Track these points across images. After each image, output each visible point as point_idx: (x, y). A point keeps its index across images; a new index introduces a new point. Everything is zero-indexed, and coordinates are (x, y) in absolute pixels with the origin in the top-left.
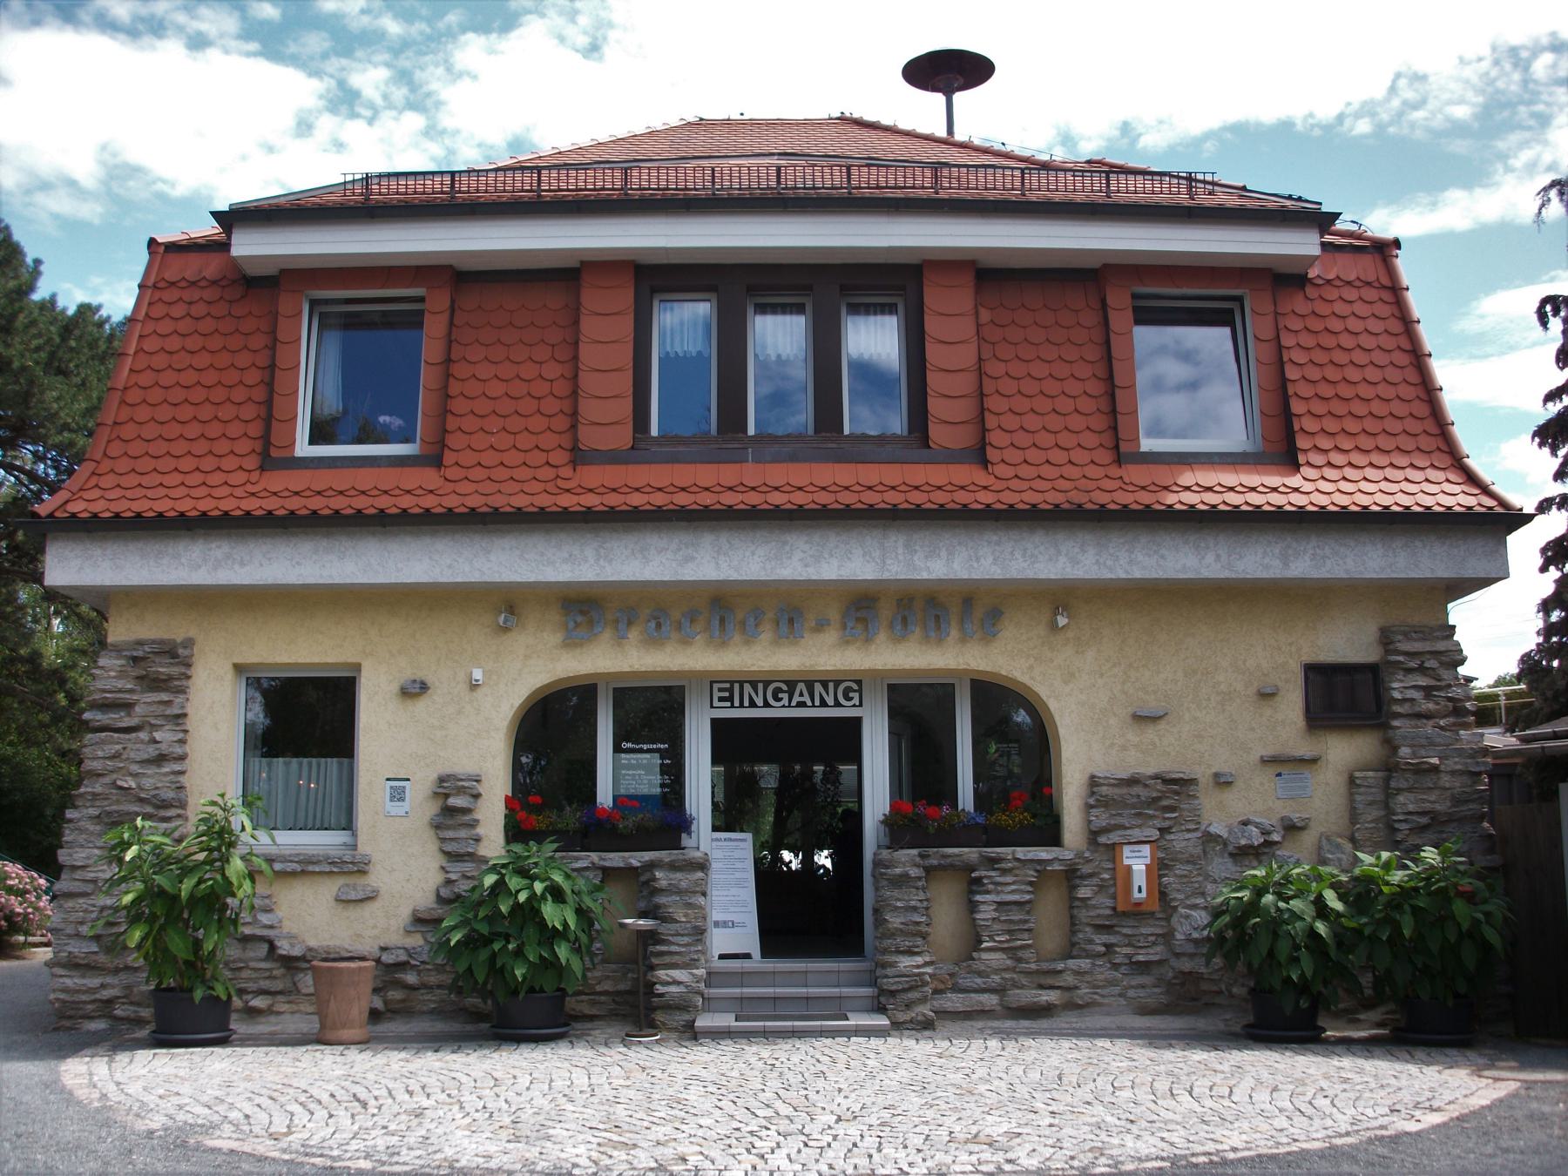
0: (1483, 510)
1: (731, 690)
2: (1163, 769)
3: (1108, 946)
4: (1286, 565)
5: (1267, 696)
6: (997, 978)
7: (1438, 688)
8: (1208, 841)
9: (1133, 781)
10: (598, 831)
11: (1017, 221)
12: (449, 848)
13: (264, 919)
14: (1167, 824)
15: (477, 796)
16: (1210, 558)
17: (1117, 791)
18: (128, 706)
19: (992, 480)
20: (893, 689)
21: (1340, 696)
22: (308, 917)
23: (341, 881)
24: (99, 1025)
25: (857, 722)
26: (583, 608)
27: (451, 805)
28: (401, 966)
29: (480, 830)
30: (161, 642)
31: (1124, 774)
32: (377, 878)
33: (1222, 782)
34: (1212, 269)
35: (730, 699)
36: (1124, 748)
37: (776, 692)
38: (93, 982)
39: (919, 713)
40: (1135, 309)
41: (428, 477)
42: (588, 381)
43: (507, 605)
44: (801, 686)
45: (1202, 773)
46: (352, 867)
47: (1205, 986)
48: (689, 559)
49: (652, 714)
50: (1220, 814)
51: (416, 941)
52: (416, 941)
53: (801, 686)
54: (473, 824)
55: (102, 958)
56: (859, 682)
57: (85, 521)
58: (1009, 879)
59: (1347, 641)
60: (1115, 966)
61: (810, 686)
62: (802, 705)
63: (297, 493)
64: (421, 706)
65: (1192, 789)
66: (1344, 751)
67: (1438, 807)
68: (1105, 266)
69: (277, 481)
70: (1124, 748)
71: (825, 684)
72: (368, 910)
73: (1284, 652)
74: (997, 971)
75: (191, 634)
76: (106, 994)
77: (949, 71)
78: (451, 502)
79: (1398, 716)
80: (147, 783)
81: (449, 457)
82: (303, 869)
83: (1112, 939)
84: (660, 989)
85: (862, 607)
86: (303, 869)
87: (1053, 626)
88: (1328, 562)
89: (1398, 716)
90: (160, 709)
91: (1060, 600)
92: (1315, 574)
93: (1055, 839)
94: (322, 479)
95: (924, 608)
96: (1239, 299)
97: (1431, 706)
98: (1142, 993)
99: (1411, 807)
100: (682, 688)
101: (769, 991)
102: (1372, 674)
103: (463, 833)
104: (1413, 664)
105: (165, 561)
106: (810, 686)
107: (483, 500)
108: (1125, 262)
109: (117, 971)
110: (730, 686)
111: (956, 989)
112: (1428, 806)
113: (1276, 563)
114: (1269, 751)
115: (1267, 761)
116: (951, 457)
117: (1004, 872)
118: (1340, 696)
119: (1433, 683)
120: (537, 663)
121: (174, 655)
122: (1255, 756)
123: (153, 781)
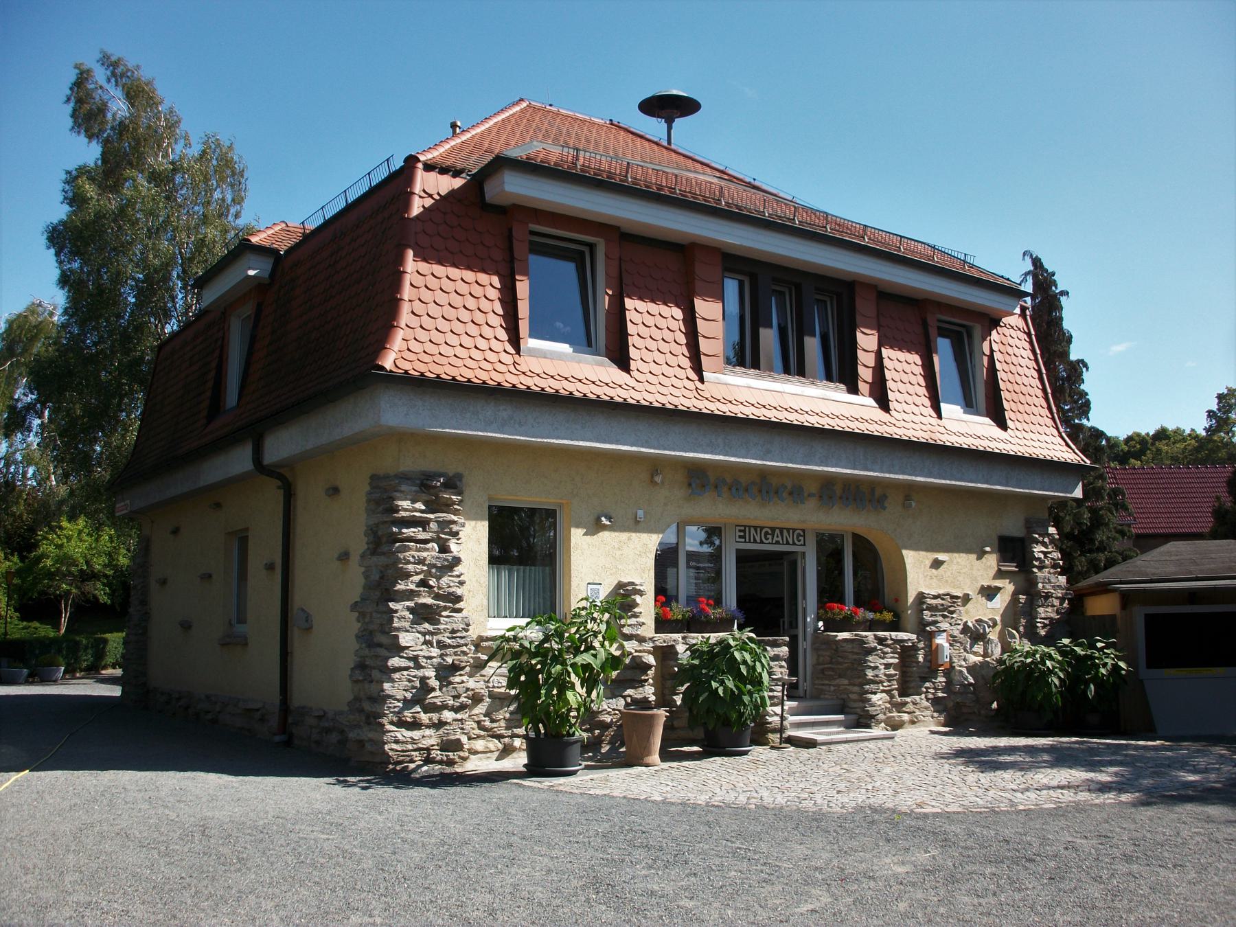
0: (607, 399)
1: (744, 531)
11: (569, 186)
19: (632, 383)
20: (818, 535)
34: (902, 297)
35: (744, 537)
37: (766, 533)
40: (939, 328)
44: (777, 531)
47: (964, 710)
53: (777, 531)
56: (804, 531)
57: (535, 394)
62: (777, 543)
68: (514, 205)
75: (460, 470)
77: (669, 107)
87: (653, 483)
96: (592, 247)
100: (551, 514)
105: (468, 415)
108: (673, 240)
110: (744, 531)
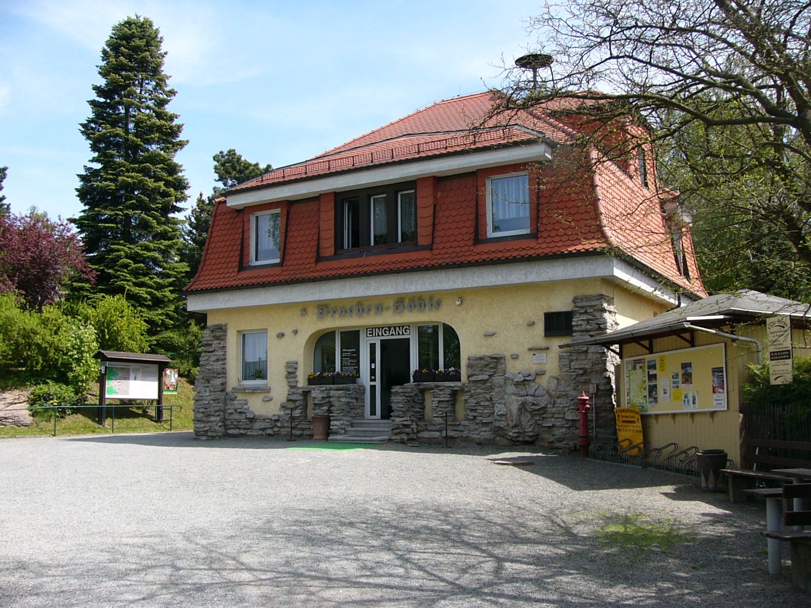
2: (496, 352)
3: (475, 417)
4: (527, 277)
5: (532, 324)
6: (438, 427)
7: (593, 320)
8: (686, 367)
9: (481, 358)
10: (336, 380)
12: (290, 384)
13: (245, 407)
14: (491, 373)
15: (296, 368)
16: (500, 277)
17: (475, 362)
18: (211, 345)
21: (557, 324)
22: (257, 406)
23: (264, 395)
24: (204, 438)
25: (409, 339)
26: (324, 308)
27: (291, 371)
28: (277, 420)
29: (298, 378)
30: (217, 325)
31: (478, 355)
32: (272, 394)
33: (515, 357)
36: (481, 346)
38: (203, 425)
39: (428, 335)
41: (532, 243)
42: (322, 234)
43: (304, 308)
44: (392, 328)
45: (508, 354)
46: (267, 390)
48: (343, 291)
49: (351, 338)
50: (515, 369)
51: (282, 413)
52: (282, 413)
53: (392, 328)
54: (296, 377)
55: (204, 419)
58: (442, 393)
59: (561, 303)
60: (477, 424)
61: (395, 328)
62: (392, 335)
63: (524, 249)
64: (283, 340)
65: (502, 361)
66: (556, 343)
67: (586, 366)
69: (480, 248)
70: (481, 346)
71: (399, 327)
72: (272, 402)
73: (536, 309)
74: (439, 424)
76: (205, 429)
78: (539, 251)
79: (576, 331)
80: (215, 367)
81: (435, 246)
82: (254, 391)
83: (475, 414)
84: (331, 427)
85: (400, 302)
86: (254, 391)
88: (542, 275)
89: (576, 331)
90: (218, 345)
91: (461, 295)
92: (537, 280)
93: (459, 380)
94: (500, 246)
95: (418, 301)
97: (588, 327)
98: (485, 434)
99: (576, 367)
101: (371, 429)
102: (568, 315)
103: (293, 380)
104: (582, 311)
106: (395, 328)
107: (591, 246)
108: (467, 171)
109: (208, 422)
110: (372, 330)
111: (427, 430)
112: (582, 366)
113: (523, 277)
114: (531, 346)
115: (530, 349)
116: (424, 248)
117: (441, 390)
118: (557, 324)
119: (591, 317)
120: (313, 325)
121: (221, 328)
122: (527, 346)
123: (217, 366)
